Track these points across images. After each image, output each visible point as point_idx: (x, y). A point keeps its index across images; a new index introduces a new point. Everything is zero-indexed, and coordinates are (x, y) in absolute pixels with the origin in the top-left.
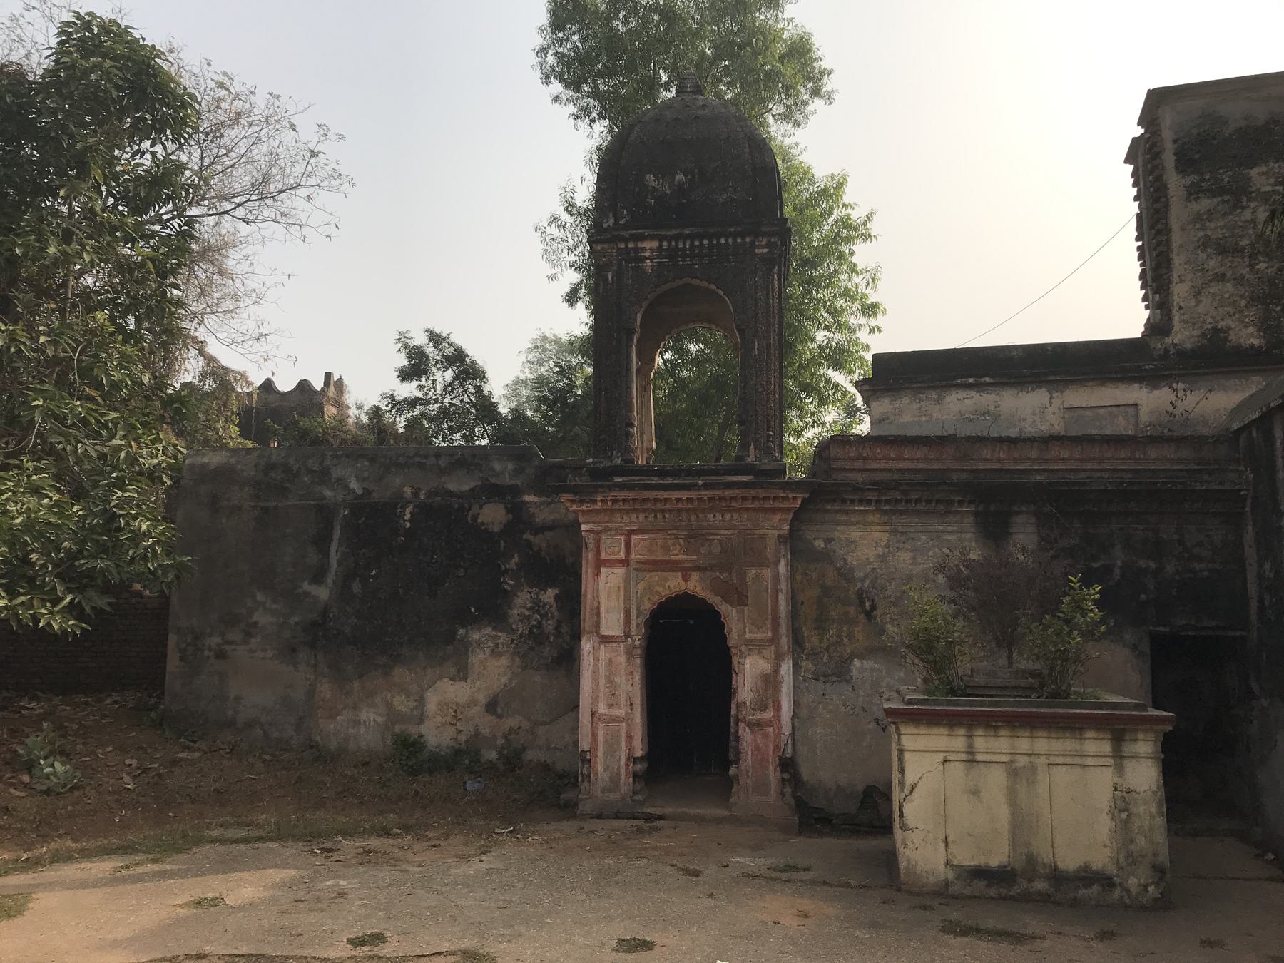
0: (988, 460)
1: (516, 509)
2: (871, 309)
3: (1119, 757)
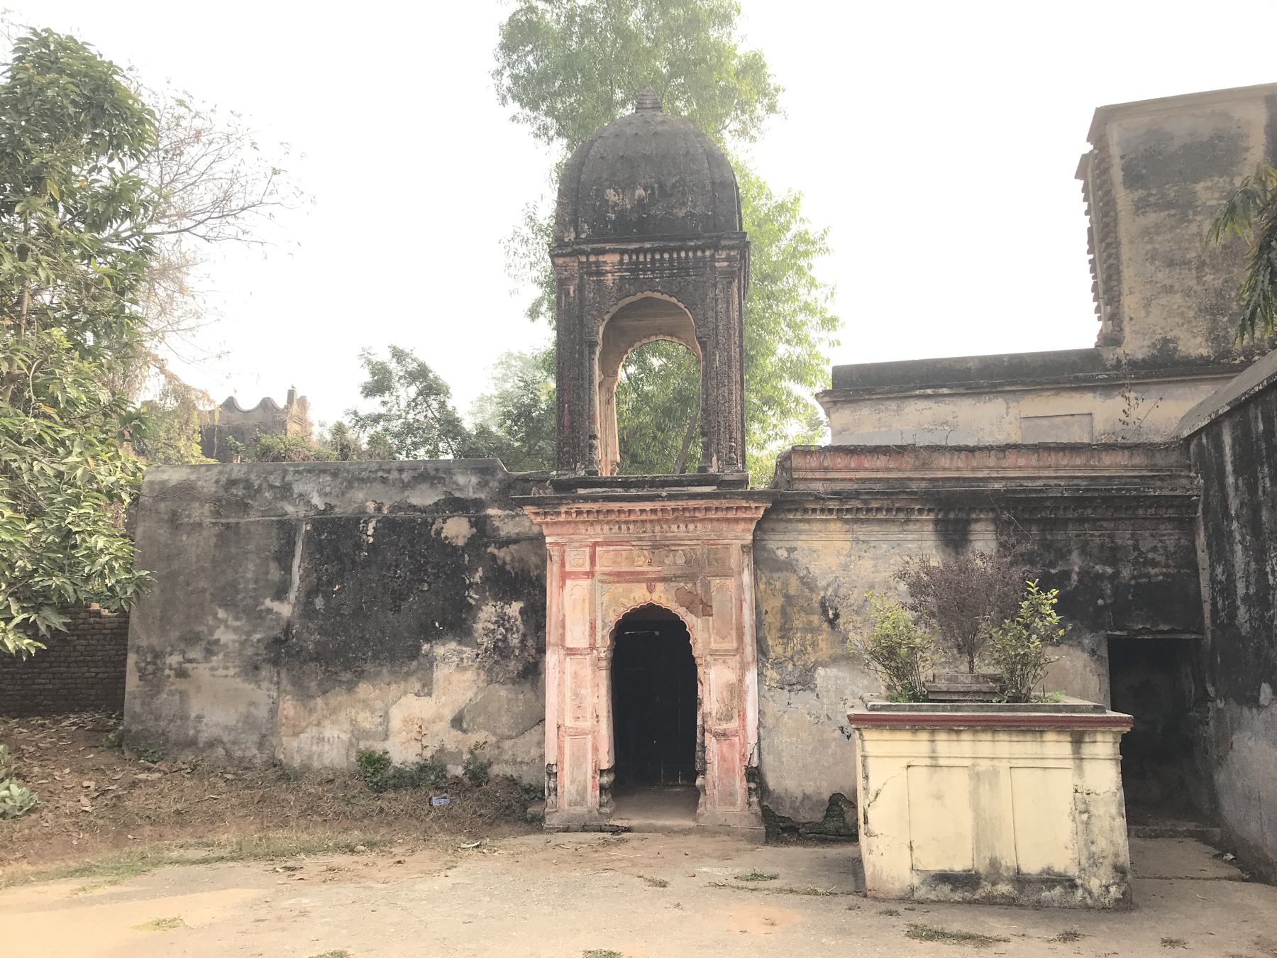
0: (946, 468)
1: (480, 524)
2: (830, 323)
3: (1079, 758)
